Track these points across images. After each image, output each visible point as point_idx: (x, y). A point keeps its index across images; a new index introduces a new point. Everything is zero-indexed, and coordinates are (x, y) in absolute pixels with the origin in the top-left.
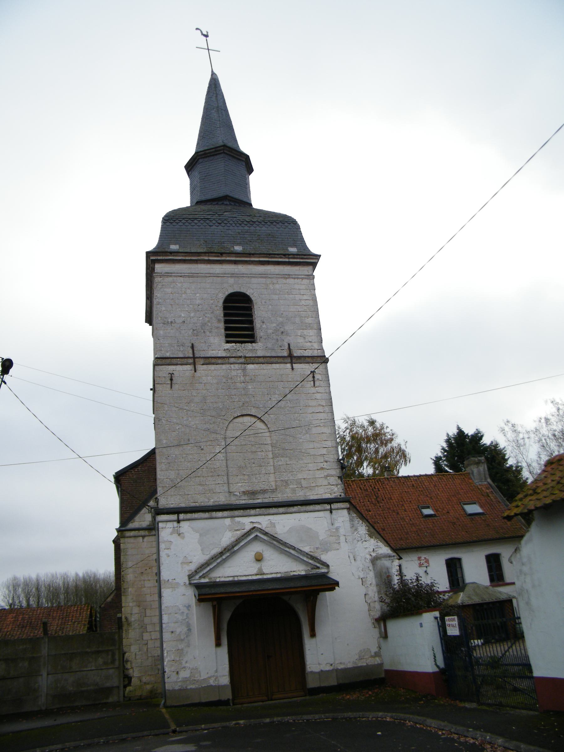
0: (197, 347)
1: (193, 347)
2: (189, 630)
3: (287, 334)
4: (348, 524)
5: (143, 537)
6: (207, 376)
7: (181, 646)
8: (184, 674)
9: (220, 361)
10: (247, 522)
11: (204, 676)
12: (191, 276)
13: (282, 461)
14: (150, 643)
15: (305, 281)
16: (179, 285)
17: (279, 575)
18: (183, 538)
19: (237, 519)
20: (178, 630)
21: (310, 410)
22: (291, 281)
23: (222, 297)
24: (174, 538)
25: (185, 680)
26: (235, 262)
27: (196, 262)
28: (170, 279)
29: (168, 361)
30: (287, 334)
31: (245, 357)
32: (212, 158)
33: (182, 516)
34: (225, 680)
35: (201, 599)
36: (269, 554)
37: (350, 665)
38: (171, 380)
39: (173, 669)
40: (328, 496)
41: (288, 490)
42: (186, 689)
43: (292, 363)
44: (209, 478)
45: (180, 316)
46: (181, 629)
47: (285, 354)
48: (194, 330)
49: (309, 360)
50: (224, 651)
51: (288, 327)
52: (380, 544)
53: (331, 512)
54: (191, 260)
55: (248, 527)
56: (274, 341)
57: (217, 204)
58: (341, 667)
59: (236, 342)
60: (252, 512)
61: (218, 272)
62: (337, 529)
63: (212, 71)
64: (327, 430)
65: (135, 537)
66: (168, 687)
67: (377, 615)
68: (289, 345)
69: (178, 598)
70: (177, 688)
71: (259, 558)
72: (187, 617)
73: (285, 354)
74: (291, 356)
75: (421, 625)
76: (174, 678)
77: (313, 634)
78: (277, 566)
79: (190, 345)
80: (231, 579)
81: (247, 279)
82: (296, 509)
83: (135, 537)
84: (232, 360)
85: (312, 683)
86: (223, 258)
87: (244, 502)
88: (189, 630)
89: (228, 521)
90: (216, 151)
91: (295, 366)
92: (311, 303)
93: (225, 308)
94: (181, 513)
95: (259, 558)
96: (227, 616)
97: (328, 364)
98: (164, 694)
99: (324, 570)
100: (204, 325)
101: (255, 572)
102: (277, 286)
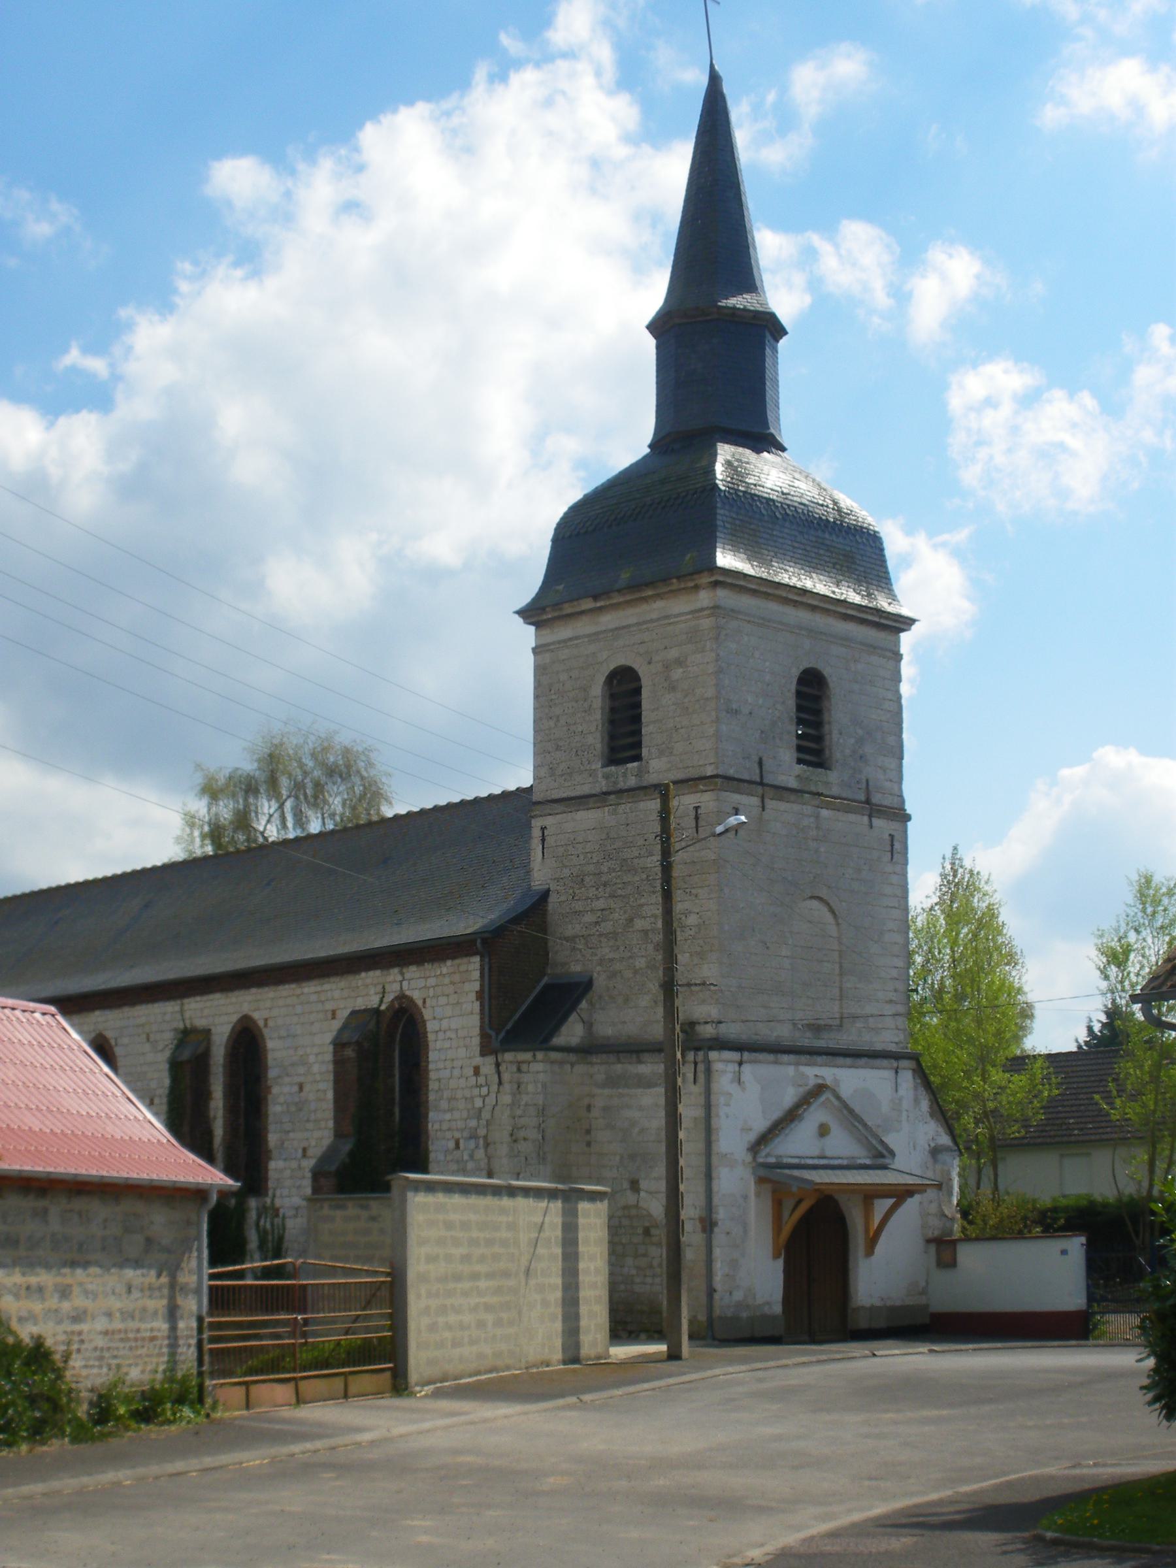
0: (768, 764)
1: (760, 763)
4: (911, 1094)
8: (738, 1296)
10: (815, 1073)
11: (759, 1301)
23: (795, 673)
24: (733, 1088)
33: (746, 1055)
34: (778, 1309)
35: (760, 1181)
37: (898, 1303)
48: (762, 732)
50: (780, 1263)
51: (868, 749)
52: (941, 1130)
53: (897, 1072)
55: (812, 1082)
56: (1151, 1087)
58: (889, 1303)
62: (900, 1099)
63: (712, 66)
67: (930, 1235)
68: (867, 781)
69: (734, 1181)
71: (823, 1131)
73: (863, 798)
74: (868, 801)
79: (757, 759)
85: (863, 1324)
89: (791, 1070)
91: (875, 821)
93: (799, 694)
95: (823, 1131)
97: (909, 824)
101: (816, 1153)
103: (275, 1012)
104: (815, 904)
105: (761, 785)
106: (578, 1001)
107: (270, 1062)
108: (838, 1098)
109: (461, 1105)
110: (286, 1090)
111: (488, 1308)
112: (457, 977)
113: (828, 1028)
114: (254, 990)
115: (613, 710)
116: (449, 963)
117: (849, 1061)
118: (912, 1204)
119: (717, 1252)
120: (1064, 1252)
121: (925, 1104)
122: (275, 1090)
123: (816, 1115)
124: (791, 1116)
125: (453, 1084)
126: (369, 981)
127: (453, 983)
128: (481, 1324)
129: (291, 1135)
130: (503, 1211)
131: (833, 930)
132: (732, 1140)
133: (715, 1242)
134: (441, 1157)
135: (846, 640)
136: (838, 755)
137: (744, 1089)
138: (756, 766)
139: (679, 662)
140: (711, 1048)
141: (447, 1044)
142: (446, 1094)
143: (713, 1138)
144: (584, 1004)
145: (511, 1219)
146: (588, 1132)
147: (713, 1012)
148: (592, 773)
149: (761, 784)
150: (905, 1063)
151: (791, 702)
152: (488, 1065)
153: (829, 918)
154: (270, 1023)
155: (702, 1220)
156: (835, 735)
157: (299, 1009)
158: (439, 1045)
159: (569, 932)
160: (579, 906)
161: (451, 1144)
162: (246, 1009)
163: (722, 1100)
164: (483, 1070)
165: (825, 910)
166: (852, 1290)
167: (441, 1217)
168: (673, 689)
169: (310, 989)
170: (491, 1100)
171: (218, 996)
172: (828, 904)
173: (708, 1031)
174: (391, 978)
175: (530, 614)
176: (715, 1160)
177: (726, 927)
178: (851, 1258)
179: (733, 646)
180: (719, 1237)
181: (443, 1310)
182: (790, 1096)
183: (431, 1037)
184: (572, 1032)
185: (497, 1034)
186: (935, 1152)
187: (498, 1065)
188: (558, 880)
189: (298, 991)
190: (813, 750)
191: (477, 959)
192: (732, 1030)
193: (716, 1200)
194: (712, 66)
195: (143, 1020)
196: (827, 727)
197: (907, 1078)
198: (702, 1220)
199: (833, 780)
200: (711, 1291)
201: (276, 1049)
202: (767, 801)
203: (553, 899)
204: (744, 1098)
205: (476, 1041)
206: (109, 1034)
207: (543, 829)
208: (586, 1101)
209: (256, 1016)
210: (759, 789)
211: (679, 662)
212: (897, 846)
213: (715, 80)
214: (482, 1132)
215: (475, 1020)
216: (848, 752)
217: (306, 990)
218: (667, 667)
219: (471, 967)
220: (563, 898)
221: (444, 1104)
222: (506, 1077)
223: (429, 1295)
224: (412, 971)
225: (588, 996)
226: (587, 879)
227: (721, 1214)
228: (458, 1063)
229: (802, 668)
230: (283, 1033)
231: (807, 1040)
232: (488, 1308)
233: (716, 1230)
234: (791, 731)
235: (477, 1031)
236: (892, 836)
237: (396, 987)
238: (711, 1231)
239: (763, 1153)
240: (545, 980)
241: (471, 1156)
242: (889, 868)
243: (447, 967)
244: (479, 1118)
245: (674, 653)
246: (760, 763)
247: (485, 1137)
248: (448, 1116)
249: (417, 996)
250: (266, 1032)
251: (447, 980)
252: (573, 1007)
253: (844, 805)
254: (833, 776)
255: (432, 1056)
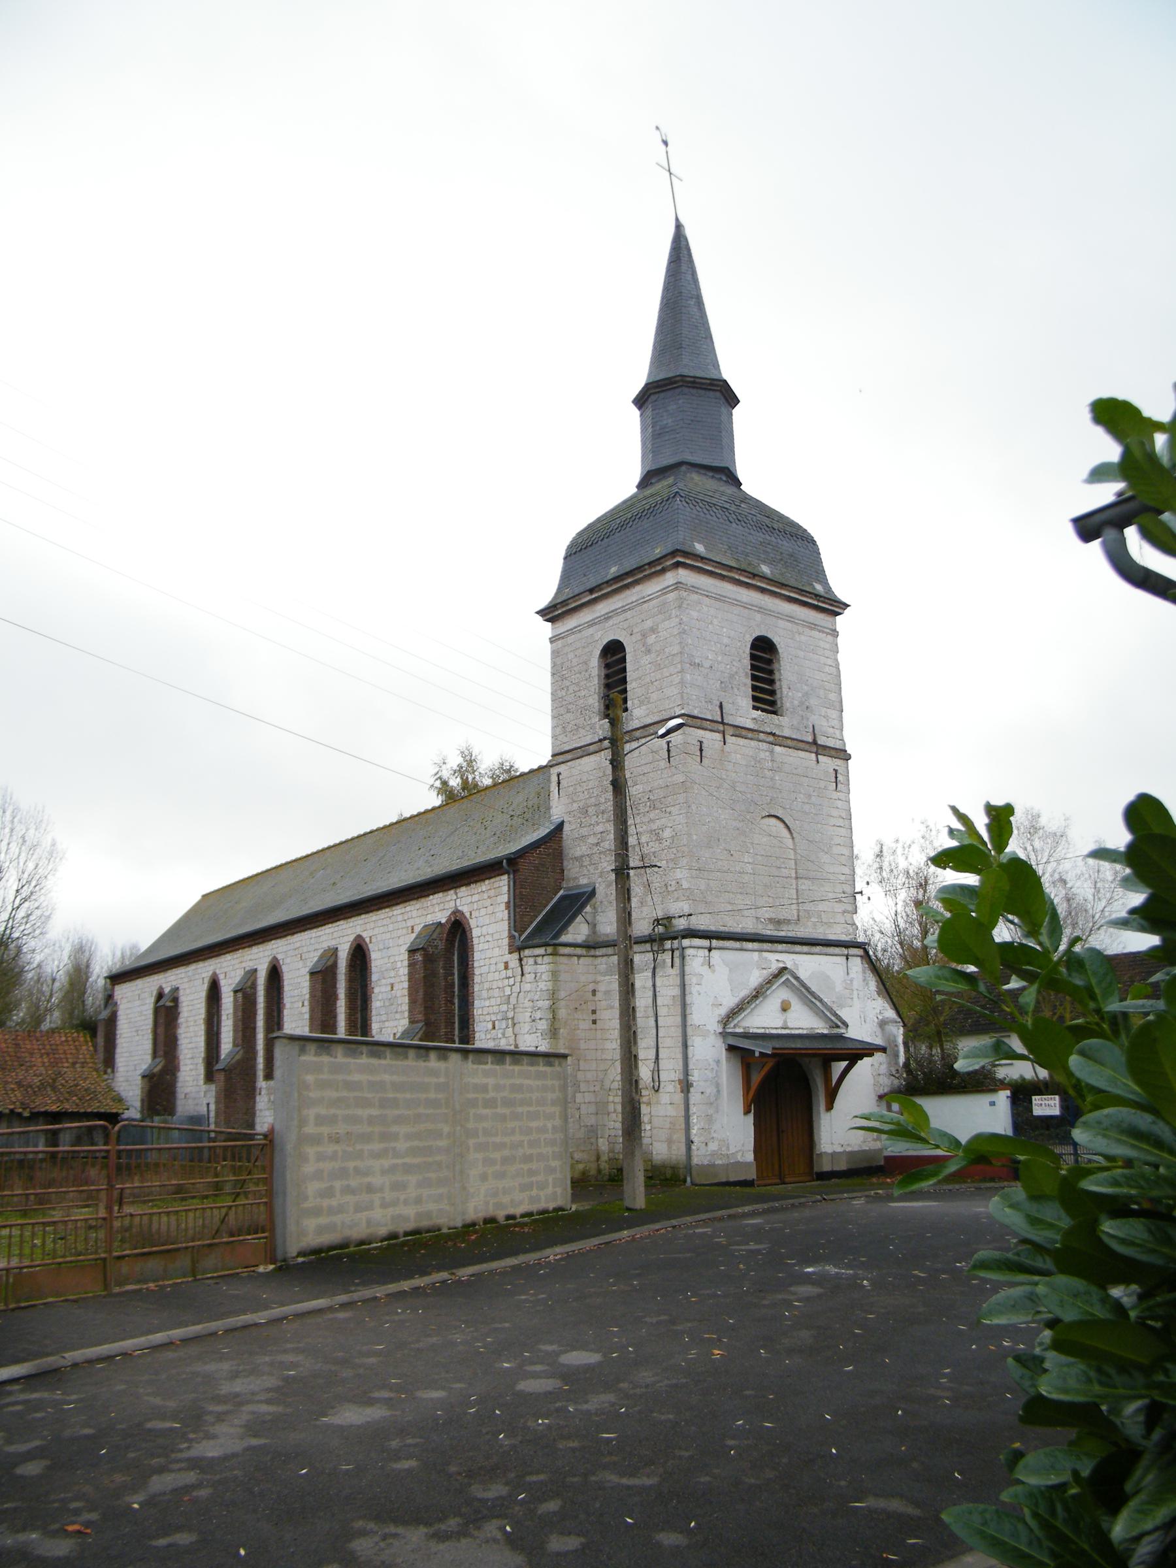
1: (721, 707)
2: (718, 1091)
3: (812, 711)
4: (861, 976)
5: (579, 956)
6: (735, 752)
7: (710, 1112)
8: (713, 1146)
9: (750, 735)
10: (775, 959)
11: (732, 1150)
12: (720, 598)
13: (804, 885)
14: (583, 1107)
15: (830, 638)
16: (705, 609)
17: (805, 1032)
18: (714, 971)
19: (765, 954)
20: (708, 1091)
21: (833, 821)
22: (815, 633)
23: (749, 640)
24: (704, 970)
25: (713, 1154)
26: (763, 591)
27: (722, 578)
28: (695, 597)
29: (699, 722)
30: (812, 711)
31: (774, 735)
32: (702, 392)
33: (715, 943)
34: (750, 1157)
35: (731, 1049)
36: (797, 1006)
38: (701, 750)
39: (702, 1139)
40: (844, 938)
41: (810, 924)
42: (714, 1165)
43: (817, 754)
44: (739, 896)
45: (707, 658)
46: (710, 1090)
47: (810, 739)
49: (833, 753)
50: (750, 1118)
51: (813, 702)
52: (886, 1005)
54: (720, 575)
55: (775, 967)
57: (713, 477)
58: (849, 1149)
59: (763, 710)
60: (780, 947)
61: (744, 600)
62: (851, 981)
63: (677, 219)
64: (846, 851)
65: (569, 955)
66: (695, 1161)
67: (881, 1092)
69: (708, 1051)
70: (706, 1162)
71: (785, 1007)
72: (717, 1076)
73: (810, 739)
74: (815, 742)
75: (993, 1104)
76: (703, 1151)
77: (830, 1107)
78: (802, 1021)
80: (762, 1031)
81: (774, 619)
82: (818, 949)
83: (569, 955)
84: (762, 736)
85: (827, 1167)
86: (754, 582)
87: (769, 933)
88: (718, 1091)
90: (711, 384)
92: (833, 670)
93: (753, 657)
94: (713, 938)
95: (785, 1007)
96: (756, 1078)
98: (689, 1167)
99: (843, 1031)
100: (732, 676)
101: (780, 1025)
102: (803, 638)
103: (376, 931)
104: (773, 821)
105: (722, 725)
106: (583, 906)
107: (374, 969)
108: (797, 978)
109: (496, 993)
110: (383, 989)
111: (408, 1169)
112: (492, 893)
113: (787, 922)
114: (363, 916)
115: (607, 676)
116: (487, 882)
117: (805, 949)
118: (864, 1065)
119: (693, 1109)
120: (993, 1104)
121: (873, 984)
122: (376, 990)
123: (779, 994)
124: (758, 994)
125: (490, 977)
126: (435, 902)
127: (489, 897)
128: (398, 1186)
129: (387, 1024)
130: (434, 1073)
131: (789, 843)
132: (706, 1014)
133: (692, 1102)
134: (483, 1036)
135: (790, 619)
136: (787, 704)
137: (714, 971)
138: (718, 709)
139: (653, 630)
140: (684, 937)
141: (486, 946)
142: (486, 986)
143: (688, 1012)
144: (588, 909)
145: (442, 1080)
146: (594, 1012)
147: (686, 908)
148: (592, 727)
149: (722, 723)
150: (853, 951)
151: (747, 662)
152: (513, 960)
153: (785, 832)
154: (374, 940)
155: (680, 1081)
156: (785, 691)
157: (391, 927)
158: (481, 947)
159: (578, 853)
160: (584, 831)
161: (490, 1026)
162: (358, 931)
163: (694, 980)
164: (511, 965)
165: (781, 825)
166: (816, 1138)
167: (340, 1077)
168: (649, 651)
169: (398, 911)
170: (516, 989)
171: (341, 922)
172: (777, 817)
173: (681, 924)
174: (448, 898)
175: (551, 614)
176: (689, 1031)
177: (695, 837)
178: (814, 1111)
179: (695, 614)
180: (695, 1097)
181: (343, 1173)
182: (755, 978)
183: (475, 941)
184: (578, 931)
185: (520, 936)
186: (883, 1024)
187: (521, 960)
188: (570, 813)
189: (390, 914)
190: (765, 694)
191: (506, 877)
192: (702, 922)
193: (691, 1066)
194: (677, 219)
195: (298, 945)
196: (778, 683)
197: (857, 965)
198: (680, 1081)
199: (784, 724)
200: (689, 1143)
201: (377, 960)
202: (727, 737)
203: (566, 828)
204: (716, 982)
205: (506, 941)
206: (279, 957)
207: (559, 775)
208: (591, 987)
209: (364, 935)
210: (721, 727)
211: (653, 630)
212: (840, 778)
213: (679, 227)
214: (510, 1015)
215: (505, 926)
216: (796, 703)
217: (395, 913)
218: (644, 636)
219: (502, 883)
220: (573, 827)
221: (485, 994)
222: (527, 969)
223: (321, 1157)
224: (463, 891)
225: (593, 901)
226: (590, 810)
227: (695, 1077)
228: (493, 961)
229: (754, 636)
230: (381, 947)
231: (769, 931)
232: (408, 1169)
233: (692, 1090)
234: (745, 682)
235: (506, 934)
236: (836, 771)
237: (452, 904)
238: (688, 1091)
239: (732, 1025)
240: (561, 892)
241: (503, 1034)
242: (835, 795)
243: (485, 886)
244: (508, 1003)
245: (649, 623)
246: (721, 707)
247: (513, 1018)
248: (487, 1003)
249: (465, 910)
250: (370, 946)
251: (485, 896)
252: (579, 911)
253: (796, 744)
254: (784, 720)
255: (477, 956)
